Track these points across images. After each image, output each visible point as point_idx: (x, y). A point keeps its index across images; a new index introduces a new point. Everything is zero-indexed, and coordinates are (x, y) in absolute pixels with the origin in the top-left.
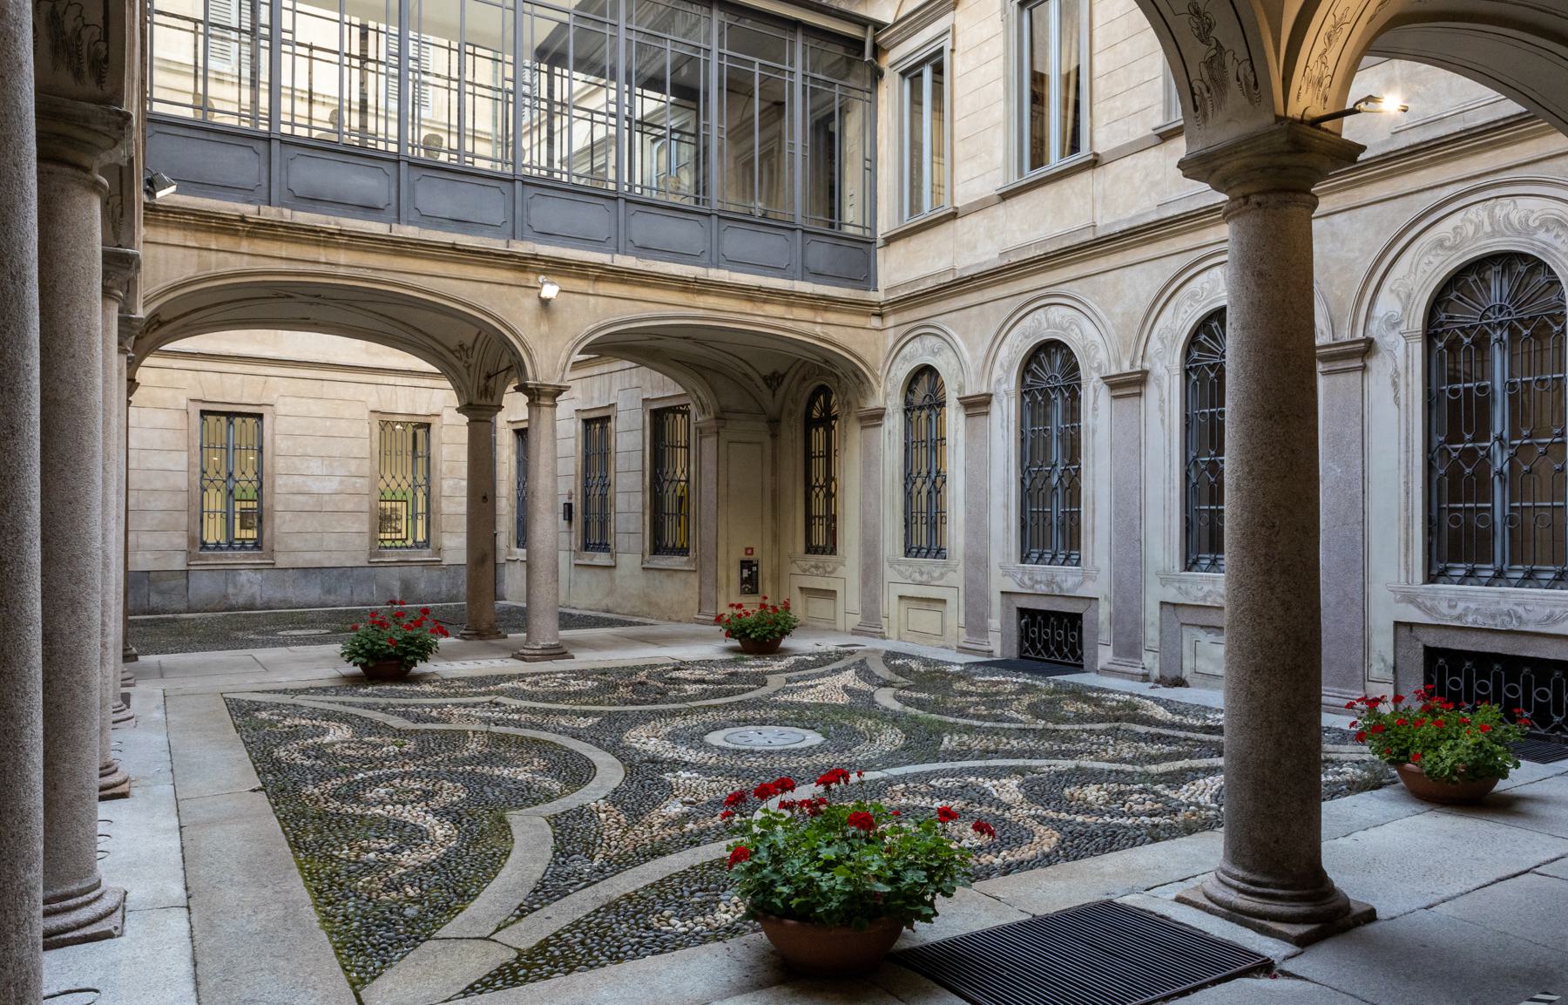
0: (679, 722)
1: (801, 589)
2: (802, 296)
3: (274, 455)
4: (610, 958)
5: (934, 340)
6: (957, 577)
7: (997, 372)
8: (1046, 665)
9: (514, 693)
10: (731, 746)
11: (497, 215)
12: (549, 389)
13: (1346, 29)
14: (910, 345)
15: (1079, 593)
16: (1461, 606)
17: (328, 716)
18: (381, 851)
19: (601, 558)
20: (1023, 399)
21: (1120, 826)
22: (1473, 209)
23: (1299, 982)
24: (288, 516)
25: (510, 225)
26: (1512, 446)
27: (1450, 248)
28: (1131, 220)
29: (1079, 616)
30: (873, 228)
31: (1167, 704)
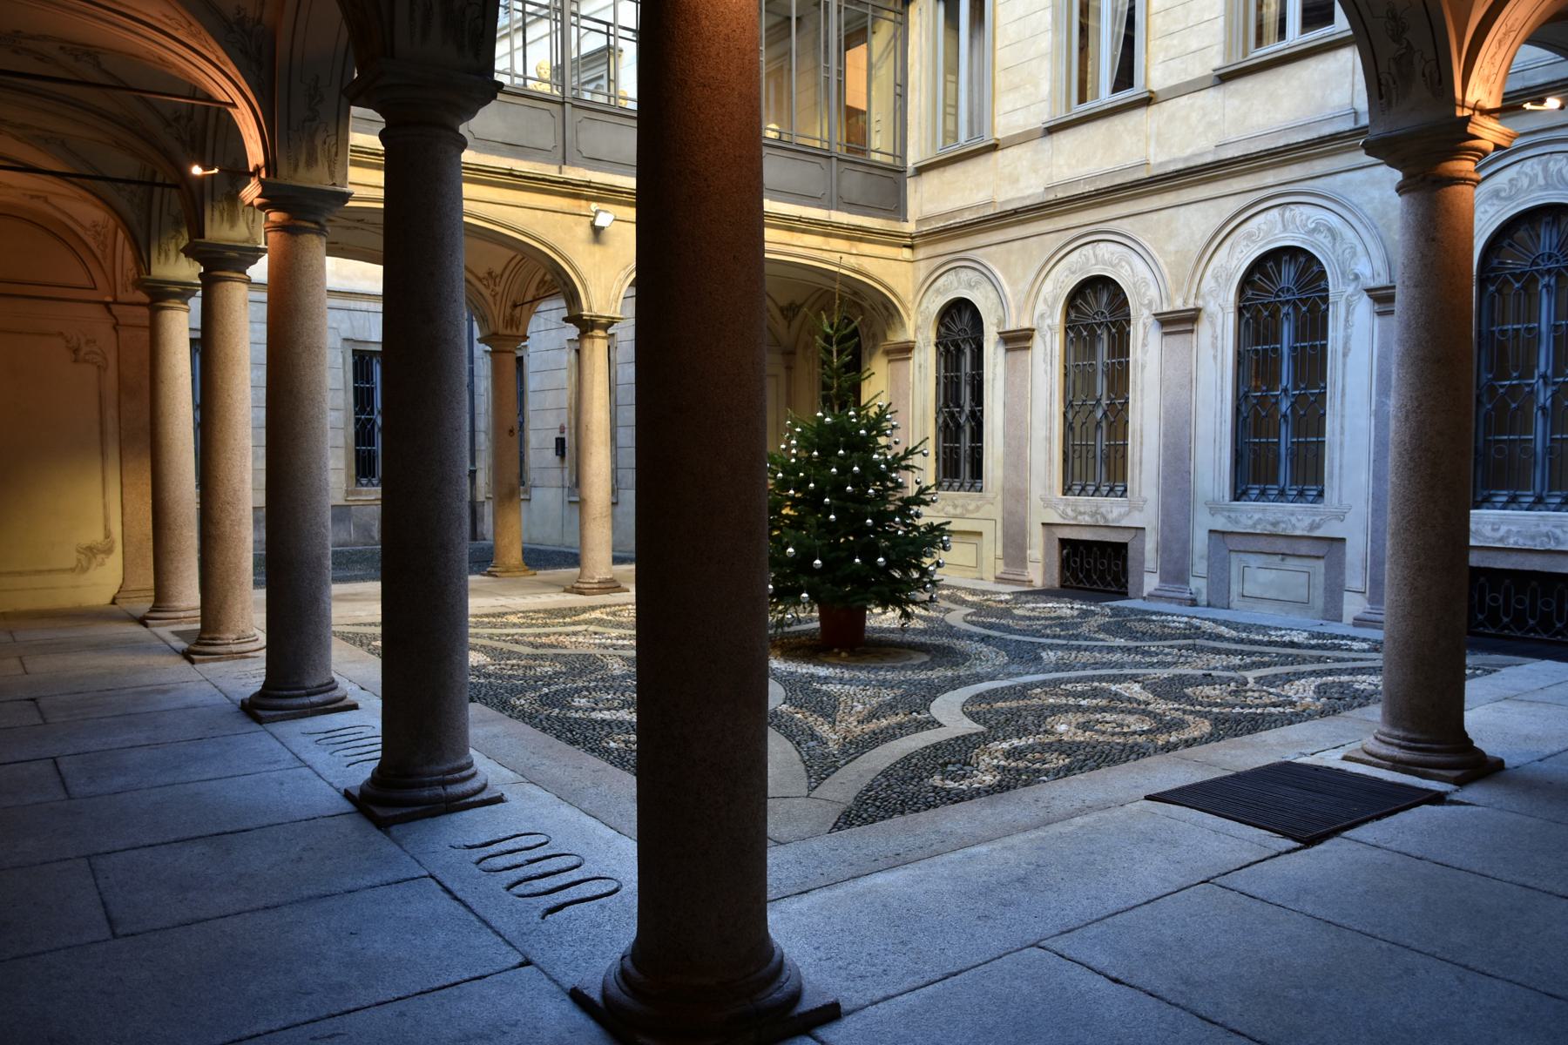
2: (839, 226)
5: (970, 273)
6: (996, 511)
7: (1041, 307)
11: (547, 139)
12: (603, 321)
13: (1513, 35)
14: (943, 279)
15: (1123, 524)
16: (1504, 529)
20: (1066, 333)
22: (1529, 162)
23: (1463, 808)
25: (560, 150)
26: (1555, 383)
27: (1505, 199)
28: (1186, 159)
30: (903, 157)
31: (1226, 624)
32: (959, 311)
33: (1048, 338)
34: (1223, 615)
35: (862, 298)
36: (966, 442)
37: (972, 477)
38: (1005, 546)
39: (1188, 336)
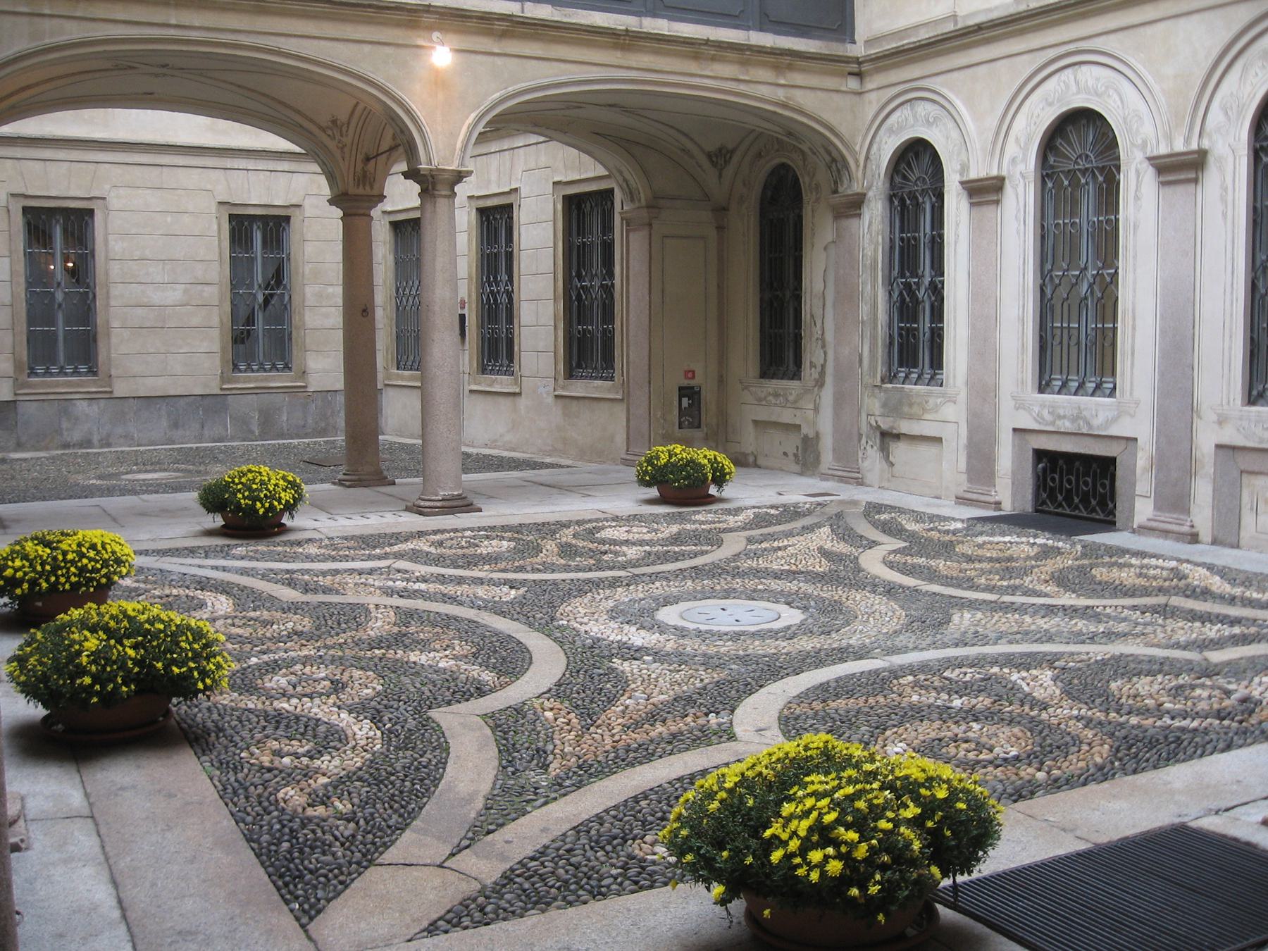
0: (621, 594)
1: (755, 422)
2: (761, 50)
3: (108, 259)
4: (590, 892)
5: (928, 106)
7: (1012, 149)
8: (1053, 519)
9: (415, 556)
10: (692, 626)
17: (203, 584)
18: (297, 756)
19: (502, 383)
20: (1044, 183)
21: (1183, 730)
24: (126, 333)
29: (1111, 461)
31: (1223, 573)
32: (917, 155)
33: (1021, 189)
34: (1225, 557)
35: (797, 139)
36: (925, 323)
37: (932, 367)
38: (969, 457)
39: (1191, 187)
